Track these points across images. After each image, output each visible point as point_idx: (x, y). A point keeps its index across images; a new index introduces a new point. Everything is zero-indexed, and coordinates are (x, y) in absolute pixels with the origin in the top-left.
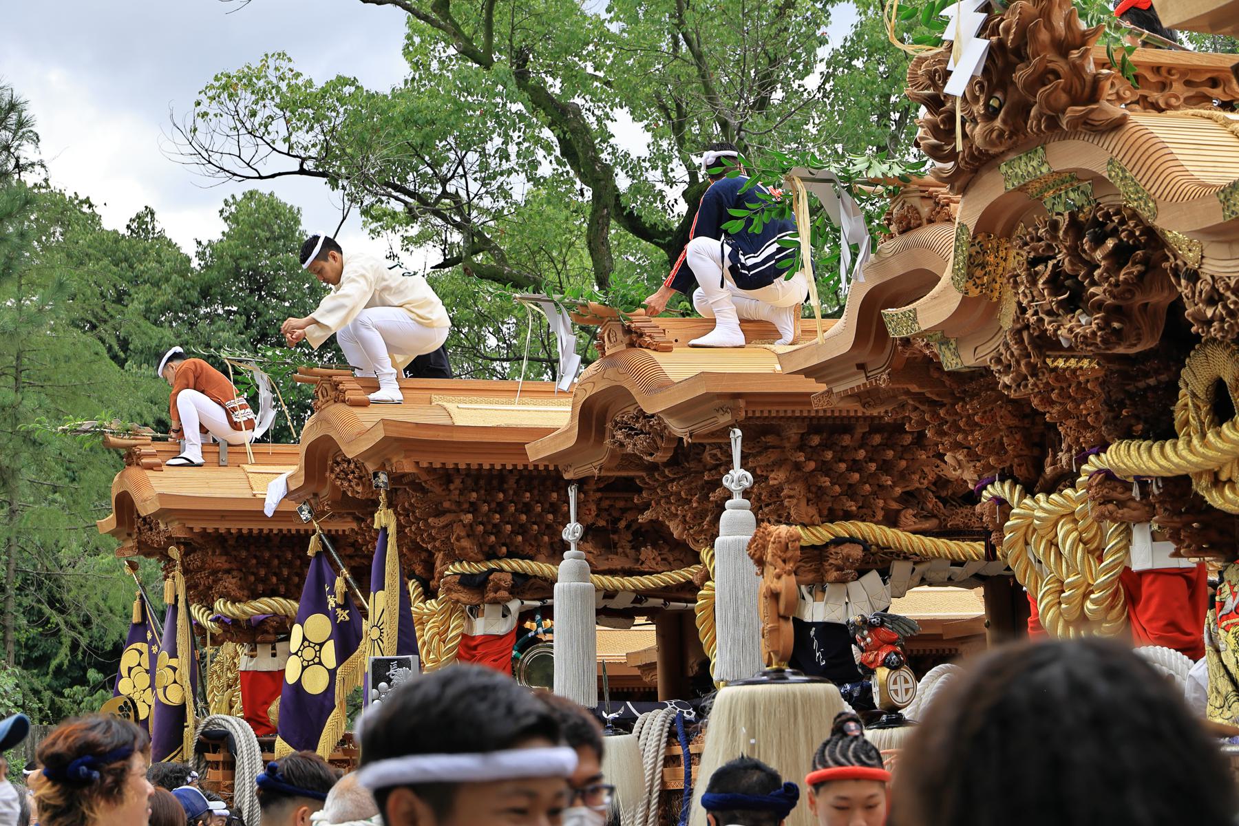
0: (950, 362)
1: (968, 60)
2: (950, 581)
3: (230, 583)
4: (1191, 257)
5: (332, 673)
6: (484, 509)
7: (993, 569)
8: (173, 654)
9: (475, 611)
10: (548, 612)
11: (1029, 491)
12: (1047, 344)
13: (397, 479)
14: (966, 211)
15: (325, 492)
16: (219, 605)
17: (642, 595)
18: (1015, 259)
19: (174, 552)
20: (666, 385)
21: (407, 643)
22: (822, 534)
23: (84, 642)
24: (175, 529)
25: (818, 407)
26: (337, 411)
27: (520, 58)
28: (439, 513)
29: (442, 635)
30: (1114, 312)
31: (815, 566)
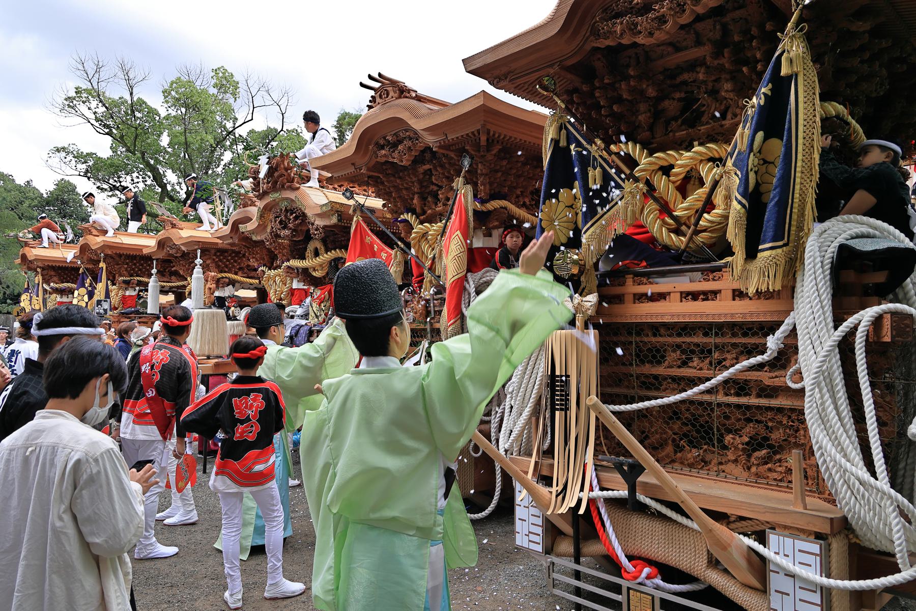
0: (254, 238)
1: (264, 170)
2: (249, 289)
3: (55, 279)
4: (312, 220)
5: (87, 303)
6: (129, 265)
7: (260, 286)
8: (38, 296)
9: (126, 289)
10: (147, 291)
11: (270, 269)
12: (278, 236)
13: (106, 255)
14: (260, 204)
15: (85, 257)
16: (52, 284)
17: (171, 287)
18: (272, 216)
19: (39, 270)
20: (181, 238)
21: (107, 295)
22: (219, 276)
23: (8, 293)
24: (40, 264)
25: (220, 246)
26: (90, 237)
27: (143, 154)
28: (118, 264)
29: (117, 295)
30: (294, 230)
31: (219, 283)
